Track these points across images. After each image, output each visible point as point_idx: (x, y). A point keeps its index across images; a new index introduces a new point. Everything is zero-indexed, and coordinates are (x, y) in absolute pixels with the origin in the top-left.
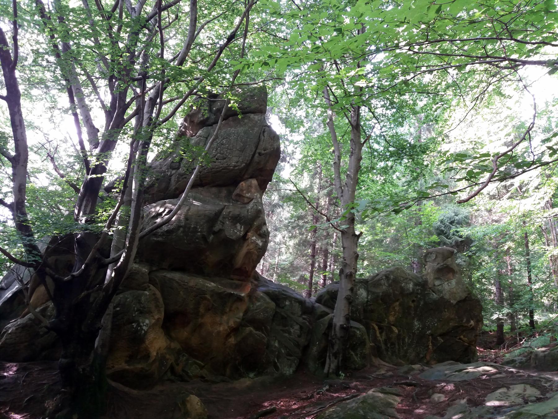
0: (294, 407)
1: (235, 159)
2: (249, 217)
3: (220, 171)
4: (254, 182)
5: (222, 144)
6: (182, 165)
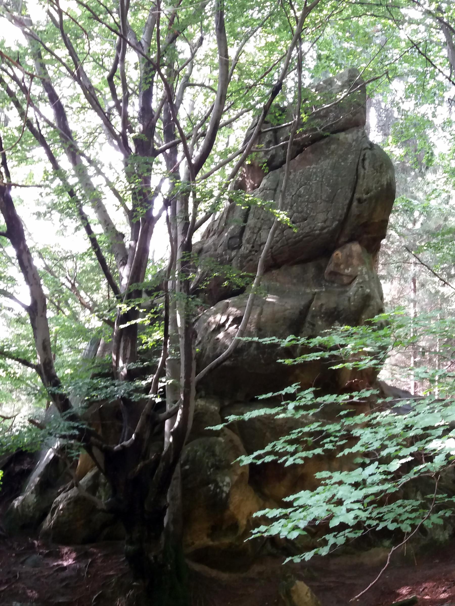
0: (443, 596)
1: (321, 217)
2: (353, 309)
3: (301, 240)
4: (356, 248)
5: (299, 196)
6: (244, 241)
